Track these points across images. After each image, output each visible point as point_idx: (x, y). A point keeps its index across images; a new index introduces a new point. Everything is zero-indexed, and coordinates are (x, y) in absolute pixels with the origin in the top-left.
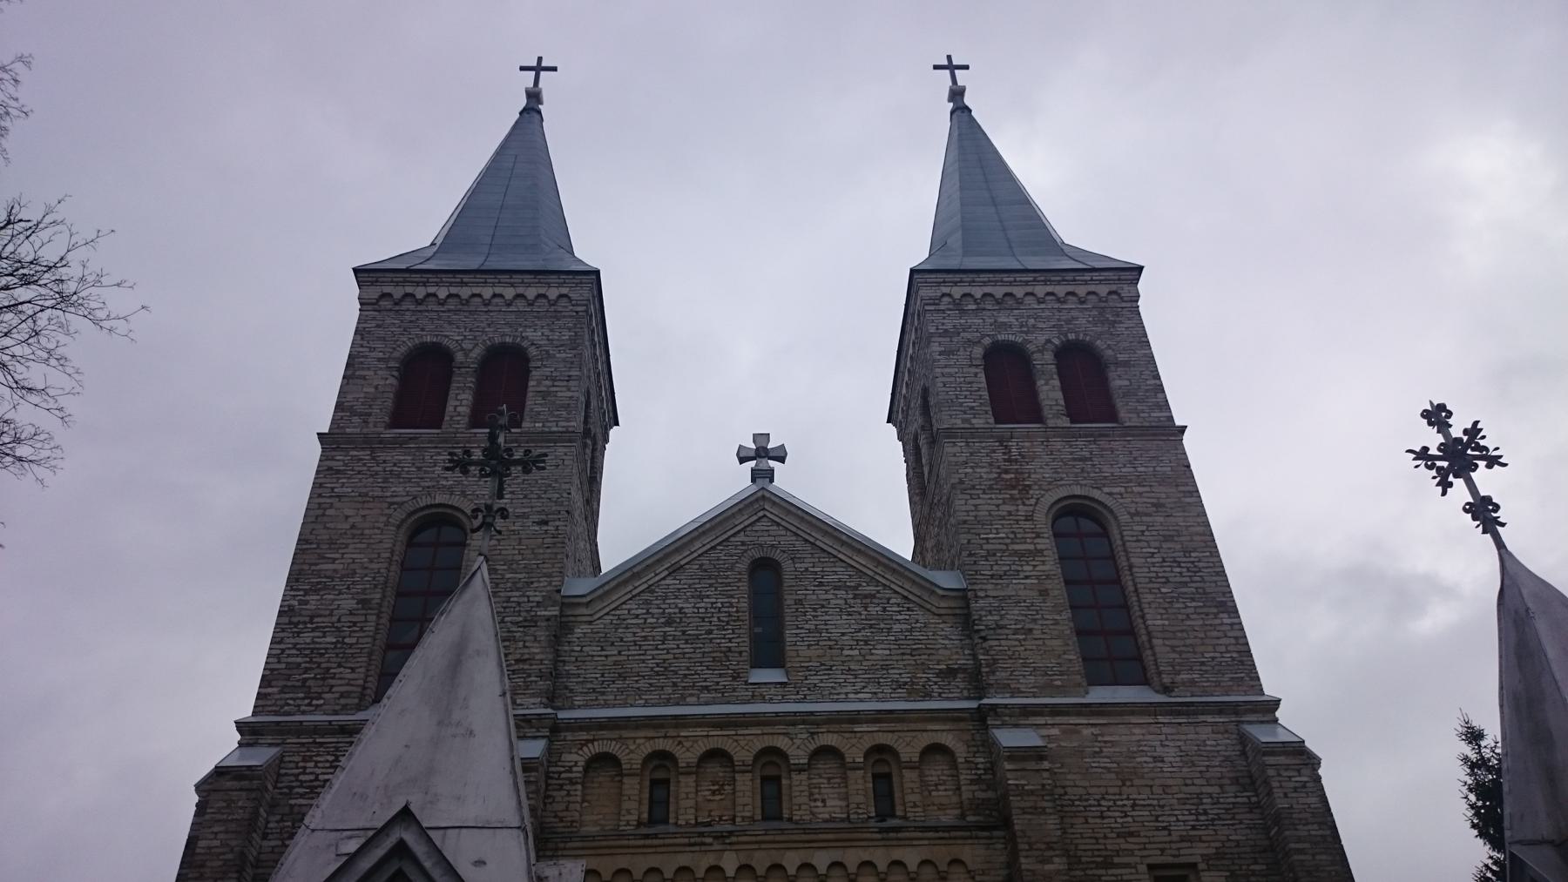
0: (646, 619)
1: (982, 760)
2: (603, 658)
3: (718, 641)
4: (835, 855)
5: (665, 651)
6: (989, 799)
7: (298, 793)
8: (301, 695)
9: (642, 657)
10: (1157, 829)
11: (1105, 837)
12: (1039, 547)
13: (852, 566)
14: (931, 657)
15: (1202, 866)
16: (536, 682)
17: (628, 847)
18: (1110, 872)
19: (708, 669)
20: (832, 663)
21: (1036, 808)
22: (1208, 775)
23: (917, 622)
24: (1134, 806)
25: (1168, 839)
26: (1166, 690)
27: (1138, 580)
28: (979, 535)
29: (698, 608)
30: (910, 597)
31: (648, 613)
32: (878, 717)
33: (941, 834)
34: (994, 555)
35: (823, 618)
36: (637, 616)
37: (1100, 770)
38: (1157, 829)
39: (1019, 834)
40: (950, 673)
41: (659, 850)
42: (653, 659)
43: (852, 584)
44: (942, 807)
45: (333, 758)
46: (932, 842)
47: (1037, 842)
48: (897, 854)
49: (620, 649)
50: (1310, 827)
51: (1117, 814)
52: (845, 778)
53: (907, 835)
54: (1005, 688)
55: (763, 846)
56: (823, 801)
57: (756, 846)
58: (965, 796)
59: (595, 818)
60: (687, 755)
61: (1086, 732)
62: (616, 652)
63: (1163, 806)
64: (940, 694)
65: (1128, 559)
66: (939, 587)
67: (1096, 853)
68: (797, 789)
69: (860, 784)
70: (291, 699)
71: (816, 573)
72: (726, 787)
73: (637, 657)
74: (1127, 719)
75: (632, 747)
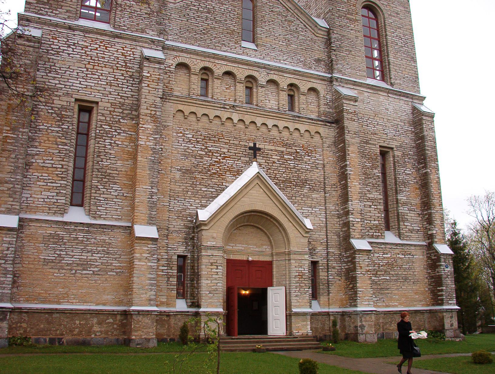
0: (198, 8)
1: (329, 97)
2: (180, 21)
3: (229, 25)
4: (276, 122)
5: (207, 25)
6: (330, 112)
7: (51, 53)
8: (48, 7)
9: (197, 25)
10: (383, 134)
11: (367, 133)
12: (357, 18)
13: (285, 7)
14: (312, 53)
15: (395, 149)
16: (155, 25)
17: (195, 103)
18: (368, 145)
19: (225, 37)
20: (275, 46)
21: (352, 119)
22: (401, 118)
23: (308, 37)
24: (378, 124)
25: (387, 138)
26: (392, 84)
27: (388, 41)
28: (336, 7)
29: (221, 9)
30: (307, 26)
31: (199, 5)
32: (295, 73)
33: (313, 122)
34: (341, 17)
35: (272, 26)
36: (195, 6)
37: (369, 109)
38: (383, 134)
39: (345, 127)
40: (318, 61)
41: (208, 107)
42: (202, 27)
43: (285, 14)
44: (312, 112)
45: (66, 40)
46: (310, 124)
47: (351, 131)
48: (298, 126)
49: (188, 19)
50: (431, 143)
51: (372, 126)
52: (278, 94)
53: (302, 120)
54: (340, 72)
55: (249, 113)
56: (269, 101)
57: (246, 113)
58: (321, 109)
59: (179, 89)
60: (219, 70)
61: (366, 94)
62: (186, 20)
63: (386, 126)
64: (315, 68)
65: (386, 32)
66: (319, 25)
67: (364, 138)
68: (260, 94)
69: (284, 97)
70: (43, 8)
71: (270, 6)
72: (232, 87)
73: (195, 24)
74: (379, 93)
75: (196, 63)
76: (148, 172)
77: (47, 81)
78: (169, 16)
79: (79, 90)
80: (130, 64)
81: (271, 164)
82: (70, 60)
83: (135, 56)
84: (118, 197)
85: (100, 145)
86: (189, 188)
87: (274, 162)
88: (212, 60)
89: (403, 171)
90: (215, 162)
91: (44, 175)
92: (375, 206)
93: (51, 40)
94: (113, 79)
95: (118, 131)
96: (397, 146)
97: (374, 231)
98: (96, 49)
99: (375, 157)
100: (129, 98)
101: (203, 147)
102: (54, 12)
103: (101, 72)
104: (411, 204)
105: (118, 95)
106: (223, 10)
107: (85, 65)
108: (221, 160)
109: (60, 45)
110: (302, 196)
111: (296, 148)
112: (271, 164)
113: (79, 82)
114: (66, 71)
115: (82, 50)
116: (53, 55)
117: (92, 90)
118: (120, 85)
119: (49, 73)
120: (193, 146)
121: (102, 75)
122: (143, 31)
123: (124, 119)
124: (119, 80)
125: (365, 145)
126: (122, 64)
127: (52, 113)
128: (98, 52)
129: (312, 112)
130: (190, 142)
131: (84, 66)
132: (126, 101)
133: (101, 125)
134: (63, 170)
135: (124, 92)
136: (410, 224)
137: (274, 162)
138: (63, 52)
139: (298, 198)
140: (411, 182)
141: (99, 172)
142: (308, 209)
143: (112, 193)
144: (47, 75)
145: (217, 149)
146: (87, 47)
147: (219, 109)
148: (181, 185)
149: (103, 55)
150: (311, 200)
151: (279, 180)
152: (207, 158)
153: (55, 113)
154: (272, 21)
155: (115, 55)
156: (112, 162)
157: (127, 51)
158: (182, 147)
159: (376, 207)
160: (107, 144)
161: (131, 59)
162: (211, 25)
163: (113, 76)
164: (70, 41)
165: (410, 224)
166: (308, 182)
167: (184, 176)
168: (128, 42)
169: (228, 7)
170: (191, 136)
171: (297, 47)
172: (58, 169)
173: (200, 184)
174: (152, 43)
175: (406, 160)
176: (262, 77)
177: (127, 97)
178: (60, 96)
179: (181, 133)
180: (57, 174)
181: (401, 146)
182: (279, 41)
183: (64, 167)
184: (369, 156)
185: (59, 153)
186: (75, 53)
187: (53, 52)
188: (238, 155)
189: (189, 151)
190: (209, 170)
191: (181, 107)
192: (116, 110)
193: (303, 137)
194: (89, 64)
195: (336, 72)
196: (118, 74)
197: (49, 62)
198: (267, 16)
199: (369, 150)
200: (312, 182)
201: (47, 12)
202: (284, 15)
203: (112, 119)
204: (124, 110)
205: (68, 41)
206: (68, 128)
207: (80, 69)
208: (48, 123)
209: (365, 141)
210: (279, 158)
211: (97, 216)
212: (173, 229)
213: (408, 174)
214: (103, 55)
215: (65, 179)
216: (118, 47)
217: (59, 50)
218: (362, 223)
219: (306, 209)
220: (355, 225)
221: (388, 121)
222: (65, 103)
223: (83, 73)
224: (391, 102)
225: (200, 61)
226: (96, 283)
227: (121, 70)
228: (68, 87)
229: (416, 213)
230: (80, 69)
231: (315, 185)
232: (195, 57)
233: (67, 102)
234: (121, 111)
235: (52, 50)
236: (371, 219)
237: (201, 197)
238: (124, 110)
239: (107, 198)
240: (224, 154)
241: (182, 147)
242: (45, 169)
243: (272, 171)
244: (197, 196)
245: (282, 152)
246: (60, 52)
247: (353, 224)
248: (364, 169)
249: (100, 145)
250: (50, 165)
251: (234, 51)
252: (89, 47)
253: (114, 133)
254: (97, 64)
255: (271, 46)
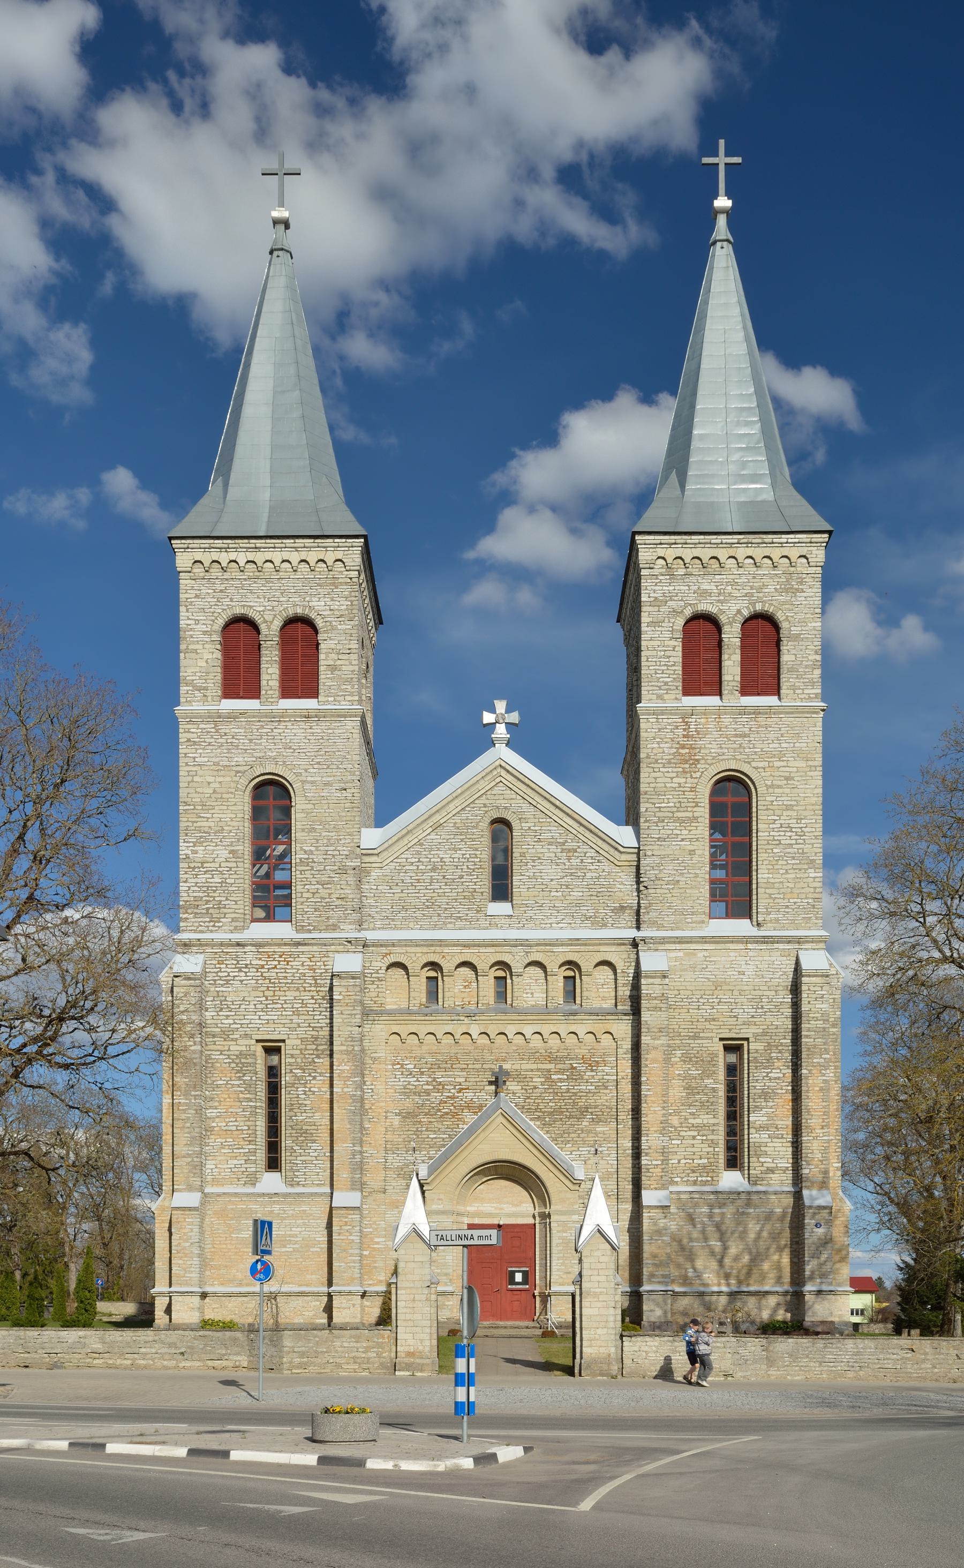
0: (418, 866)
2: (392, 895)
3: (467, 884)
8: (208, 920)
9: (417, 895)
12: (696, 814)
18: (696, 1042)
20: (543, 902)
22: (770, 984)
23: (604, 871)
29: (453, 858)
30: (601, 851)
34: (663, 821)
41: (433, 1022)
44: (604, 998)
49: (402, 888)
55: (494, 1022)
56: (532, 994)
57: (490, 1022)
67: (690, 1030)
73: (413, 895)
75: (414, 959)
76: (349, 1126)
77: (219, 1021)
78: (374, 891)
79: (259, 1028)
80: (322, 979)
81: (531, 1091)
82: (243, 989)
83: (327, 967)
84: (318, 1158)
85: (291, 1096)
86: (411, 1136)
87: (535, 1088)
88: (438, 949)
89: (765, 1074)
90: (448, 1097)
91: (228, 1140)
92: (703, 1136)
93: (218, 966)
94: (300, 1005)
95: (313, 1075)
96: (756, 1035)
97: (698, 1175)
98: (275, 967)
99: (709, 1059)
100: (324, 1029)
101: (430, 1080)
102: (217, 924)
103: (285, 998)
104: (776, 1128)
105: (310, 1026)
106: (456, 860)
107: (263, 992)
108: (456, 1094)
109: (229, 970)
110: (579, 1132)
111: (571, 1062)
112: (531, 1091)
113: (257, 1017)
114: (240, 1004)
115: (257, 971)
116: (222, 985)
117: (276, 1026)
118: (310, 1013)
119: (220, 1011)
120: (415, 1079)
121: (286, 1003)
122: (335, 928)
123: (319, 1058)
124: (308, 1005)
125: (692, 1041)
126: (310, 982)
127: (229, 1063)
128: (278, 971)
129: (604, 998)
130: (410, 1074)
131: (261, 994)
132: (321, 1033)
133: (291, 1070)
134: (250, 1132)
135: (317, 1021)
136: (770, 1160)
137: (535, 1088)
138: (233, 980)
139: (573, 1135)
140: (779, 1091)
141: (293, 1129)
142: (588, 1149)
143: (311, 1154)
144: (218, 1015)
145: (450, 1079)
146: (263, 967)
147: (450, 1022)
148: (402, 1133)
149: (284, 975)
150: (593, 1135)
151: (544, 1112)
152: (435, 1094)
153: (233, 1062)
154: (539, 858)
155: (300, 971)
156: (308, 1115)
157: (315, 962)
158: (401, 1083)
159: (704, 1138)
160: (300, 1093)
161: (321, 973)
162: (438, 891)
163: (300, 1001)
164: (241, 962)
165: (770, 1160)
166: (590, 1110)
167: (404, 1121)
168: (315, 948)
169: (464, 852)
170: (412, 1066)
171: (581, 894)
172: (245, 1132)
173: (427, 1130)
174: (349, 944)
175: (773, 1055)
176: (517, 961)
177: (321, 1027)
178: (236, 1040)
179: (398, 1064)
180: (243, 1138)
181: (765, 1033)
182: (550, 891)
183: (251, 1128)
184: (697, 1058)
185: (243, 1111)
186: (248, 978)
187: (221, 982)
188: (482, 1084)
189: (411, 1087)
190: (439, 1110)
191: (395, 1029)
192: (308, 1047)
193: (583, 1044)
194: (268, 989)
195: (645, 926)
196: (306, 997)
197: (218, 996)
198: (530, 851)
199: (699, 1049)
200: (597, 1110)
201: (208, 927)
202: (560, 843)
203: (304, 1061)
204: (317, 1045)
205: (238, 963)
206: (251, 1079)
207: (258, 999)
208: (226, 1076)
209: (692, 1034)
210: (543, 1080)
211: (294, 1183)
212: (392, 1191)
213: (775, 1078)
214: (284, 975)
215: (253, 1143)
216: (303, 958)
217: (228, 978)
218: (663, 1166)
219: (585, 1149)
220: (651, 1170)
221: (742, 993)
222: (244, 1048)
223: (261, 1003)
224: (752, 959)
225: (420, 955)
226: (296, 1261)
227: (309, 991)
228: (245, 1026)
229: (785, 1141)
230: (258, 999)
231: (601, 1113)
232: (413, 949)
233: (246, 1045)
234: (314, 1047)
235: (220, 980)
236: (694, 1157)
237: (428, 1146)
238: (317, 1045)
239: (305, 1161)
240: (460, 1085)
241: (401, 1083)
242: (229, 1132)
243: (532, 1101)
244: (423, 1146)
245: (549, 1071)
246: (230, 980)
247: (648, 1169)
248: (686, 1081)
249: (291, 1096)
250: (234, 1128)
251: (475, 926)
252: (266, 967)
253: (307, 1078)
254: (278, 989)
255: (536, 903)
